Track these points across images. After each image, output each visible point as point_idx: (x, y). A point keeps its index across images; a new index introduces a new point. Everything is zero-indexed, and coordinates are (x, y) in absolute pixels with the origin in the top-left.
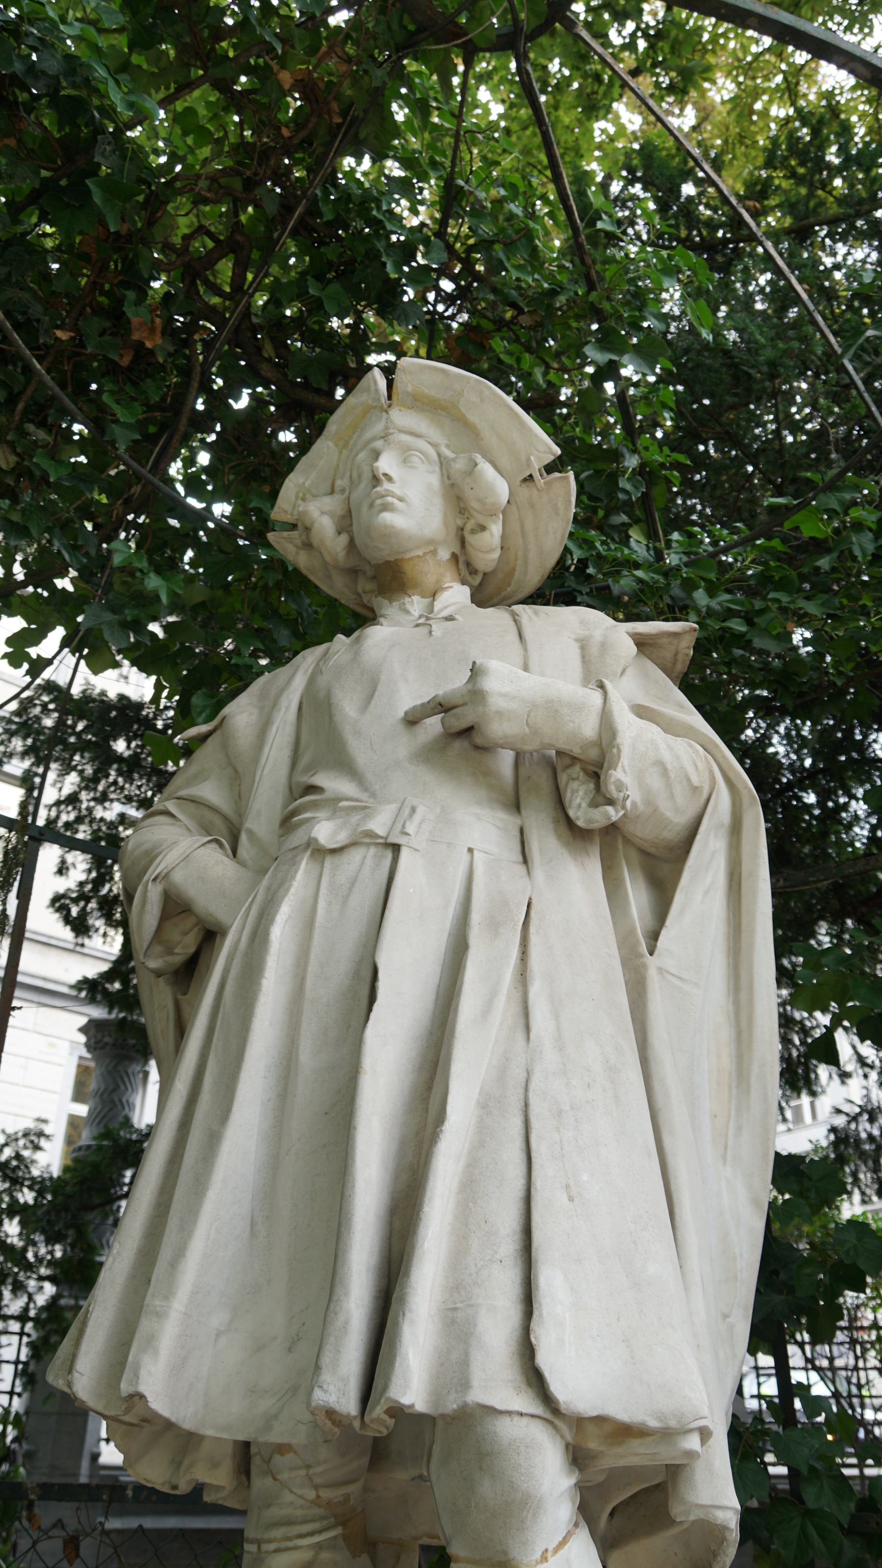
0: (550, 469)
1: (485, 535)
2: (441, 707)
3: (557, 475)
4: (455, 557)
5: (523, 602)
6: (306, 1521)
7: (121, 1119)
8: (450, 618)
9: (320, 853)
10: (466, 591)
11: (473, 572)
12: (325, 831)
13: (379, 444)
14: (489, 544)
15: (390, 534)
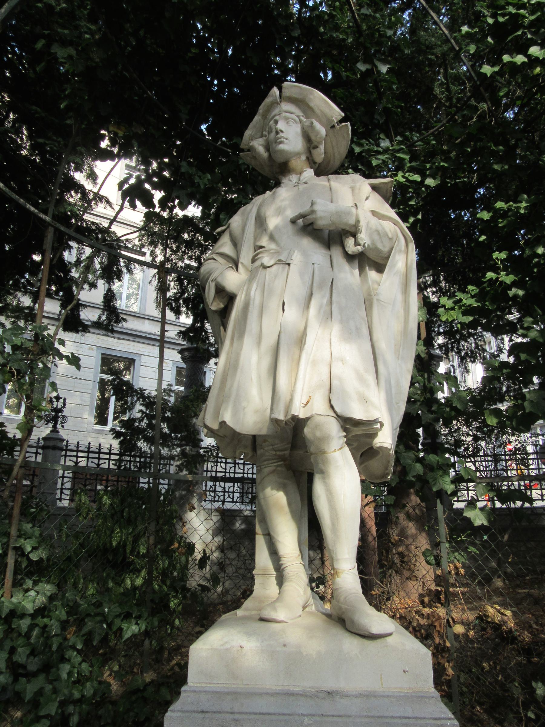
0: (341, 121)
1: (318, 149)
2: (302, 216)
3: (344, 124)
4: (308, 158)
5: (333, 173)
6: (273, 459)
7: (199, 384)
8: (306, 183)
9: (265, 267)
10: (312, 171)
11: (315, 163)
12: (266, 260)
13: (277, 118)
14: (319, 154)
15: (282, 151)
